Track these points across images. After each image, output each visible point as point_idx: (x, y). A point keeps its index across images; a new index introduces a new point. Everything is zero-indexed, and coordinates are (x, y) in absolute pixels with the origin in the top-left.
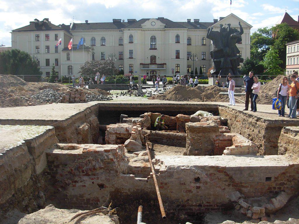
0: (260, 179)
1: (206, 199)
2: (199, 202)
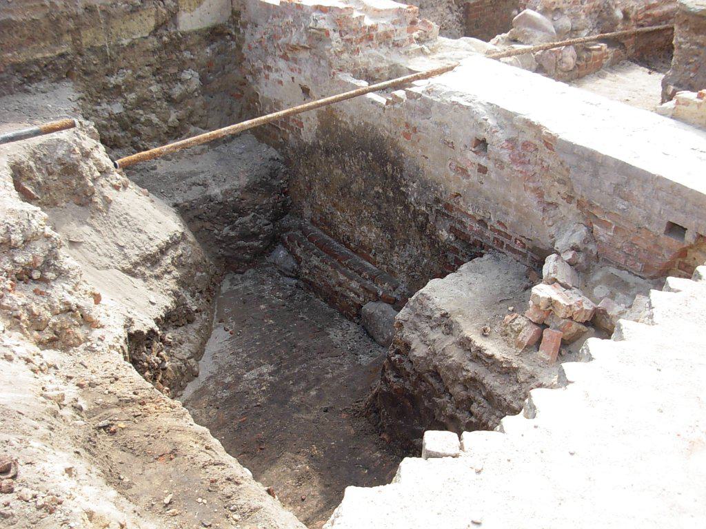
0: (648, 218)
1: (498, 213)
2: (481, 213)
